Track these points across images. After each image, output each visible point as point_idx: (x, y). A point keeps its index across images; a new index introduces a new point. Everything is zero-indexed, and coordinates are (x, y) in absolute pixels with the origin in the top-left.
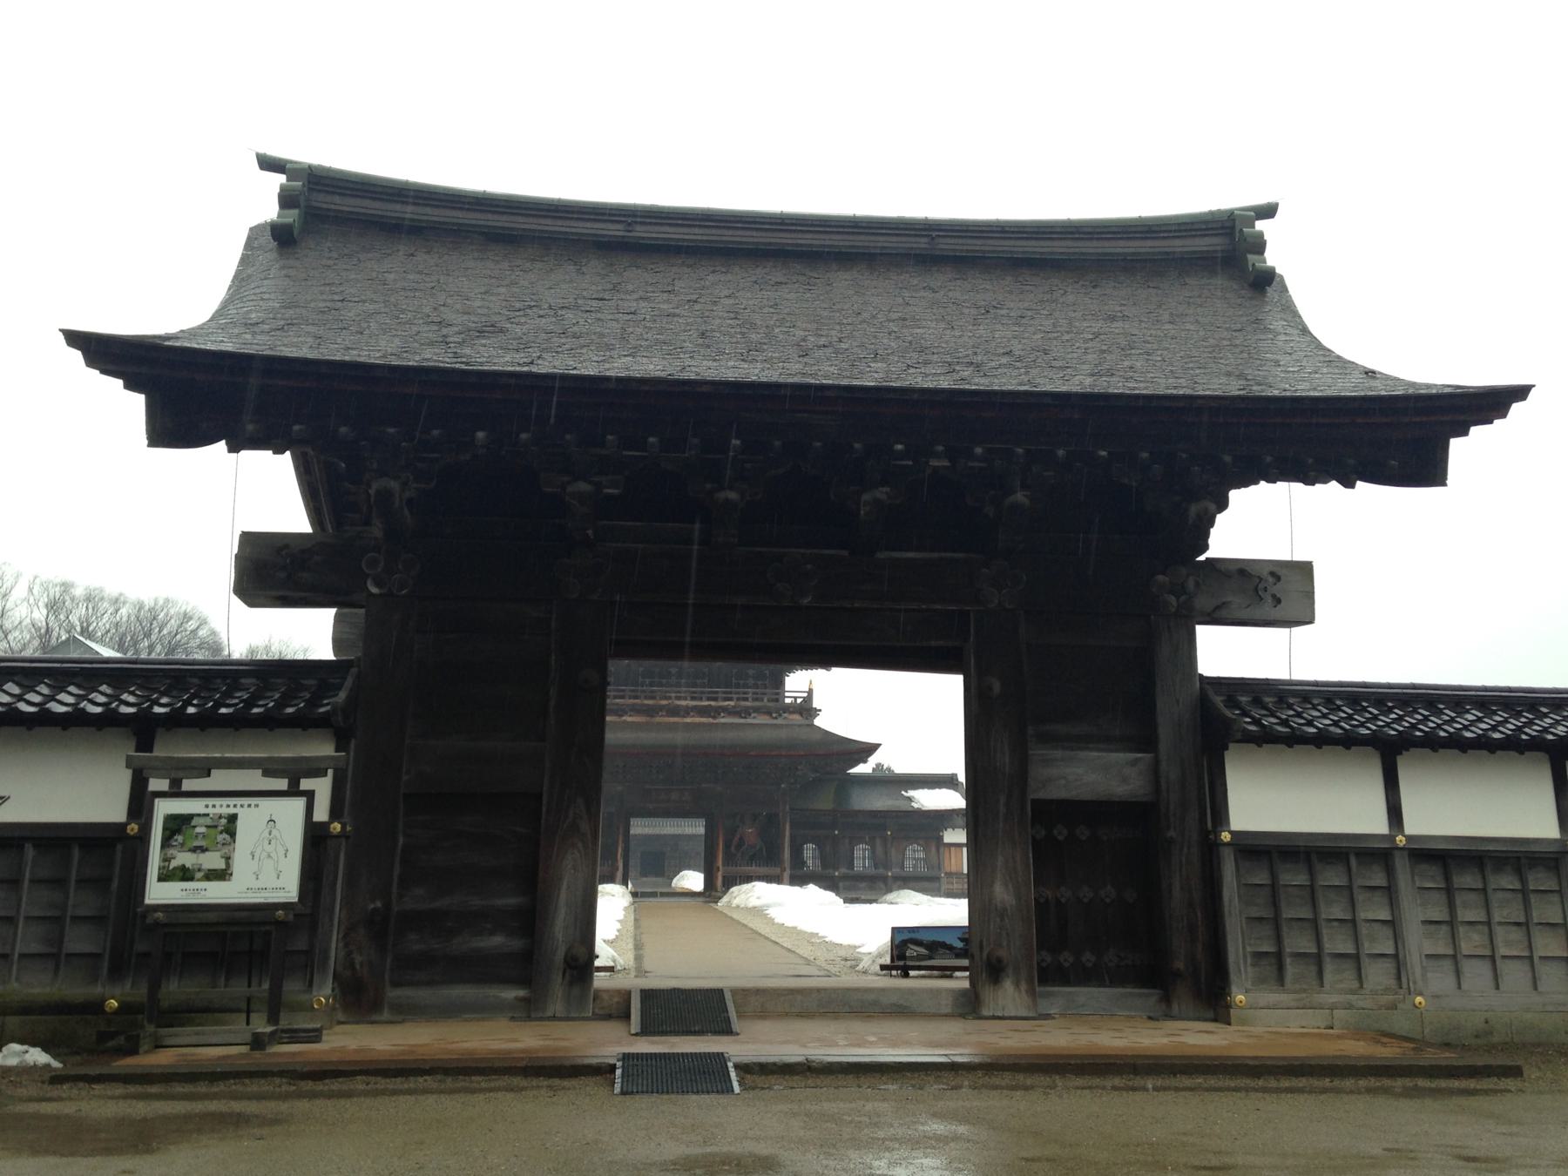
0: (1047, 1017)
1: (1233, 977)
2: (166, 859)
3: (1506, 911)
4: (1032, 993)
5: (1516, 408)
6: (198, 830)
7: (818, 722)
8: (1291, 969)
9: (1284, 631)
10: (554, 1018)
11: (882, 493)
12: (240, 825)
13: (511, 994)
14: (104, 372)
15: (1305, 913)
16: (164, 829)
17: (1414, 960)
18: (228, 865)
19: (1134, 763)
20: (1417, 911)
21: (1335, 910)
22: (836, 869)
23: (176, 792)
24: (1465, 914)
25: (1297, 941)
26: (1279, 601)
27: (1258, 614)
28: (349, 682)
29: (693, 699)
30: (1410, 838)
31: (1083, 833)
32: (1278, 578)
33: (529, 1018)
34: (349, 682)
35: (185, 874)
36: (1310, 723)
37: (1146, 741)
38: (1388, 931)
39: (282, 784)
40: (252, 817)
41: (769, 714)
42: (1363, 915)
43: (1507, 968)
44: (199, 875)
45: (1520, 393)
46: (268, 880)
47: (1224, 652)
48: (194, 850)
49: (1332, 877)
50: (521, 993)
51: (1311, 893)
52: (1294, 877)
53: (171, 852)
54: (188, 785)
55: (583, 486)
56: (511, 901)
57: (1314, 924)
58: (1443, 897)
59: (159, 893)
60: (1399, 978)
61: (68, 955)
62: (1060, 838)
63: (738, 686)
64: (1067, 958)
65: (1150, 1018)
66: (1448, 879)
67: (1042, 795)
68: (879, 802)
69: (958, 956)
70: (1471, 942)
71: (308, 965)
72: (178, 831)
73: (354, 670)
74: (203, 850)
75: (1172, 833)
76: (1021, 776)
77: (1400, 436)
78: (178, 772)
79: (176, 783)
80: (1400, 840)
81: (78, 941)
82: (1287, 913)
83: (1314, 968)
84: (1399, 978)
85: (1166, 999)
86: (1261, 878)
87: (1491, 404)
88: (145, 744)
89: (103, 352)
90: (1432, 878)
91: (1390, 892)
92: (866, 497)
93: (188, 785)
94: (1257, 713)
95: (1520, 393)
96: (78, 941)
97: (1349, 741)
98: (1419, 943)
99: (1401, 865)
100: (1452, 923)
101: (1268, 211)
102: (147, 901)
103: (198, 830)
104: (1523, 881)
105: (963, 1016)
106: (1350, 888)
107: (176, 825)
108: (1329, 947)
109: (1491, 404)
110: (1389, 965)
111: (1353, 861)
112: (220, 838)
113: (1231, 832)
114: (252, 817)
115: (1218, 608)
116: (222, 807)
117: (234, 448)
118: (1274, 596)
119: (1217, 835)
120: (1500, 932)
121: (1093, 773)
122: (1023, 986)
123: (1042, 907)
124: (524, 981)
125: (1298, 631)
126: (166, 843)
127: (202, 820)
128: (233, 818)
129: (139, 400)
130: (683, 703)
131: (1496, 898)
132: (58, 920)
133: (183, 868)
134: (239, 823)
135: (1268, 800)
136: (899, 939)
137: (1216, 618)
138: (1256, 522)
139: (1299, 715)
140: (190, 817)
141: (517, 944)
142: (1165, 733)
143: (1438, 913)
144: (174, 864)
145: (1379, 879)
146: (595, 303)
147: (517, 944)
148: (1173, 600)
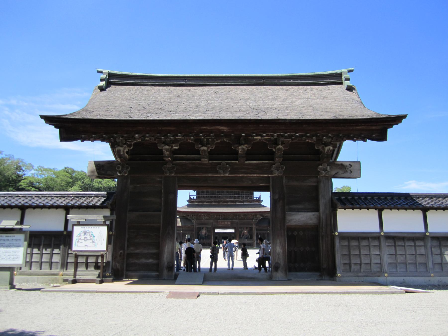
0: (291, 280)
1: (338, 269)
4: (286, 274)
8: (353, 266)
9: (355, 180)
10: (165, 280)
11: (245, 147)
14: (49, 124)
15: (357, 253)
19: (314, 215)
21: (364, 252)
24: (398, 252)
26: (351, 172)
29: (230, 198)
30: (385, 233)
32: (351, 166)
33: (158, 280)
37: (317, 210)
45: (404, 117)
47: (339, 184)
51: (359, 247)
52: (354, 243)
56: (154, 251)
57: (360, 255)
58: (393, 248)
62: (295, 235)
63: (241, 195)
65: (317, 280)
67: (289, 224)
73: (115, 194)
76: (284, 218)
80: (382, 234)
82: (352, 252)
85: (321, 276)
86: (346, 243)
87: (397, 120)
88: (67, 213)
89: (49, 120)
91: (379, 247)
92: (240, 147)
95: (404, 117)
97: (10, 207)
99: (382, 240)
100: (396, 255)
104: (415, 243)
109: (397, 120)
111: (370, 240)
113: (338, 232)
115: (336, 173)
117: (82, 141)
118: (350, 171)
123: (290, 253)
124: (157, 271)
125: (358, 179)
130: (228, 199)
135: (349, 221)
141: (155, 262)
143: (393, 252)
148: (323, 172)
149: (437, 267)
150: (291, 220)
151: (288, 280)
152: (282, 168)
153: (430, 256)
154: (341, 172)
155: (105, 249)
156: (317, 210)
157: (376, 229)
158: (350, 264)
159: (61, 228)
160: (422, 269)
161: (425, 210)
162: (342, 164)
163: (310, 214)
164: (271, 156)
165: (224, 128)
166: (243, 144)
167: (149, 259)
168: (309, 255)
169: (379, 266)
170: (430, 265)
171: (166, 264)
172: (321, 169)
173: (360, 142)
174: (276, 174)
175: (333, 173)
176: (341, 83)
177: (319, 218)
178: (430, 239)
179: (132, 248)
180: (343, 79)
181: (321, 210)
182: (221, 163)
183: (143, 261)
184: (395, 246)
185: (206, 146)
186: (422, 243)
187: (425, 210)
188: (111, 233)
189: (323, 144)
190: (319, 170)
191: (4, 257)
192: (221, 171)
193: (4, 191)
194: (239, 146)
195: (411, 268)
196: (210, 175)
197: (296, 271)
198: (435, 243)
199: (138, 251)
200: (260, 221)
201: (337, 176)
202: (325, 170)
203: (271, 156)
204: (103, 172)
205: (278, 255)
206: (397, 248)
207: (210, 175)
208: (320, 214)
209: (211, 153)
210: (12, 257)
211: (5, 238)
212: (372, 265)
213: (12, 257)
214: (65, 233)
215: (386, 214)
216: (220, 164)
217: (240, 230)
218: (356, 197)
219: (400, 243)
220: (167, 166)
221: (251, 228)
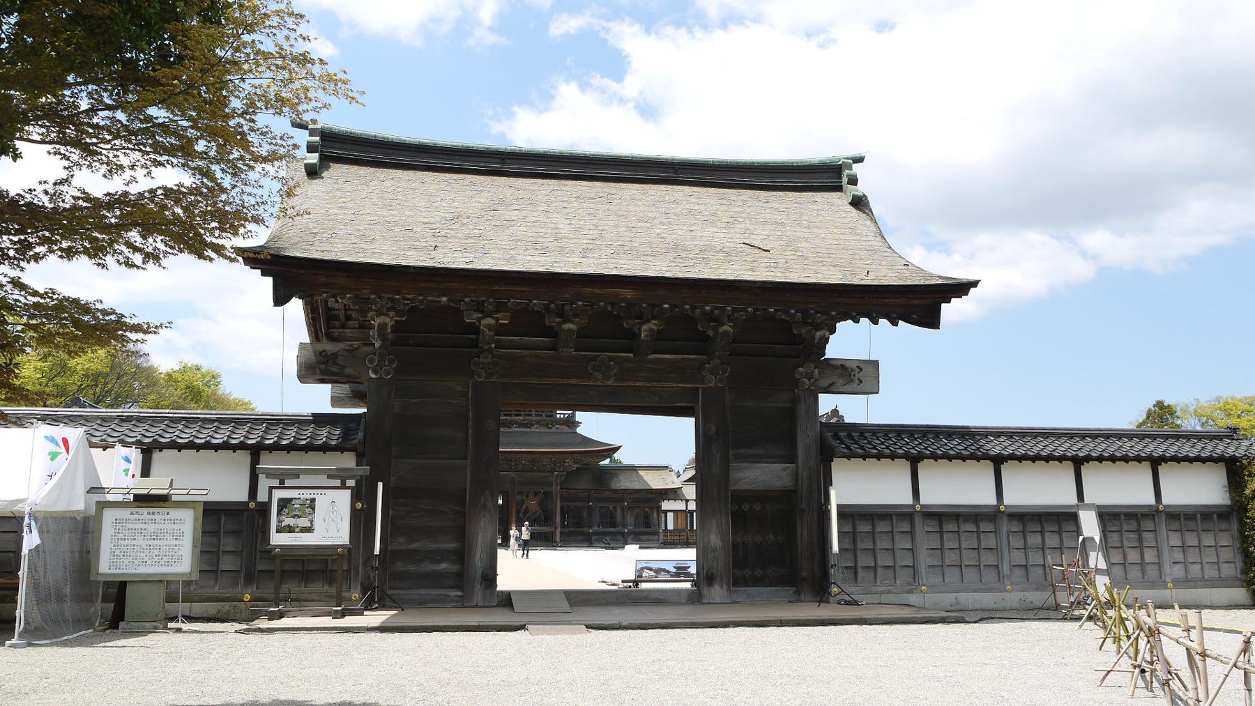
2: (280, 522)
3: (969, 541)
4: (729, 590)
5: (972, 290)
7: (579, 430)
8: (861, 573)
10: (476, 606)
11: (653, 325)
17: (923, 569)
19: (784, 470)
21: (883, 543)
22: (590, 527)
23: (282, 487)
24: (947, 545)
25: (865, 560)
27: (848, 388)
28: (362, 427)
30: (922, 506)
31: (757, 507)
34: (362, 427)
35: (290, 529)
36: (875, 448)
37: (792, 459)
38: (910, 554)
39: (338, 483)
40: (324, 500)
41: (547, 425)
42: (898, 546)
45: (975, 284)
48: (294, 517)
49: (883, 527)
50: (459, 593)
54: (288, 483)
55: (490, 321)
56: (452, 545)
58: (938, 535)
64: (748, 572)
66: (941, 527)
67: (736, 487)
68: (625, 483)
70: (951, 557)
71: (348, 575)
75: (803, 506)
77: (920, 303)
78: (282, 478)
79: (282, 482)
80: (1002, 508)
81: (227, 563)
82: (860, 545)
85: (798, 593)
90: (932, 526)
91: (912, 533)
92: (645, 327)
94: (848, 441)
95: (975, 284)
96: (227, 563)
98: (925, 559)
99: (918, 520)
101: (859, 160)
104: (978, 527)
105: (693, 603)
107: (284, 504)
108: (880, 563)
109: (961, 288)
114: (324, 500)
115: (831, 385)
116: (307, 494)
121: (762, 474)
123: (735, 546)
124: (460, 587)
126: (279, 514)
128: (313, 500)
129: (269, 281)
131: (963, 536)
132: (216, 553)
135: (855, 486)
137: (826, 391)
138: (849, 340)
139: (869, 443)
140: (291, 499)
141: (455, 568)
143: (937, 544)
145: (906, 527)
146: (492, 213)
147: (455, 568)
149: (1019, 573)
152: (725, 371)
153: (1006, 551)
154: (840, 381)
156: (792, 459)
157: (907, 499)
158: (855, 569)
159: (241, 495)
160: (990, 576)
161: (998, 461)
163: (778, 467)
164: (702, 344)
165: (628, 293)
166: (648, 321)
168: (772, 550)
169: (910, 571)
170: (1006, 568)
171: (479, 574)
172: (801, 374)
174: (712, 381)
175: (824, 383)
176: (839, 188)
177: (796, 476)
179: (401, 540)
180: (845, 180)
183: (429, 567)
184: (941, 533)
185: (572, 322)
186: (990, 527)
187: (998, 461)
188: (359, 505)
189: (811, 325)
190: (797, 376)
191: (146, 559)
192: (598, 375)
193: (19, 405)
194: (641, 324)
195: (970, 575)
196: (573, 382)
197: (747, 586)
198: (1016, 527)
199: (413, 546)
200: (573, 475)
201: (832, 388)
202: (810, 376)
203: (702, 344)
204: (334, 369)
205: (714, 550)
206: (945, 536)
207: (573, 382)
209: (581, 333)
210: (166, 559)
211: (145, 516)
212: (898, 569)
213: (166, 559)
215: (927, 472)
216: (595, 358)
217: (518, 498)
218: (854, 434)
219: (950, 527)
221: (548, 495)
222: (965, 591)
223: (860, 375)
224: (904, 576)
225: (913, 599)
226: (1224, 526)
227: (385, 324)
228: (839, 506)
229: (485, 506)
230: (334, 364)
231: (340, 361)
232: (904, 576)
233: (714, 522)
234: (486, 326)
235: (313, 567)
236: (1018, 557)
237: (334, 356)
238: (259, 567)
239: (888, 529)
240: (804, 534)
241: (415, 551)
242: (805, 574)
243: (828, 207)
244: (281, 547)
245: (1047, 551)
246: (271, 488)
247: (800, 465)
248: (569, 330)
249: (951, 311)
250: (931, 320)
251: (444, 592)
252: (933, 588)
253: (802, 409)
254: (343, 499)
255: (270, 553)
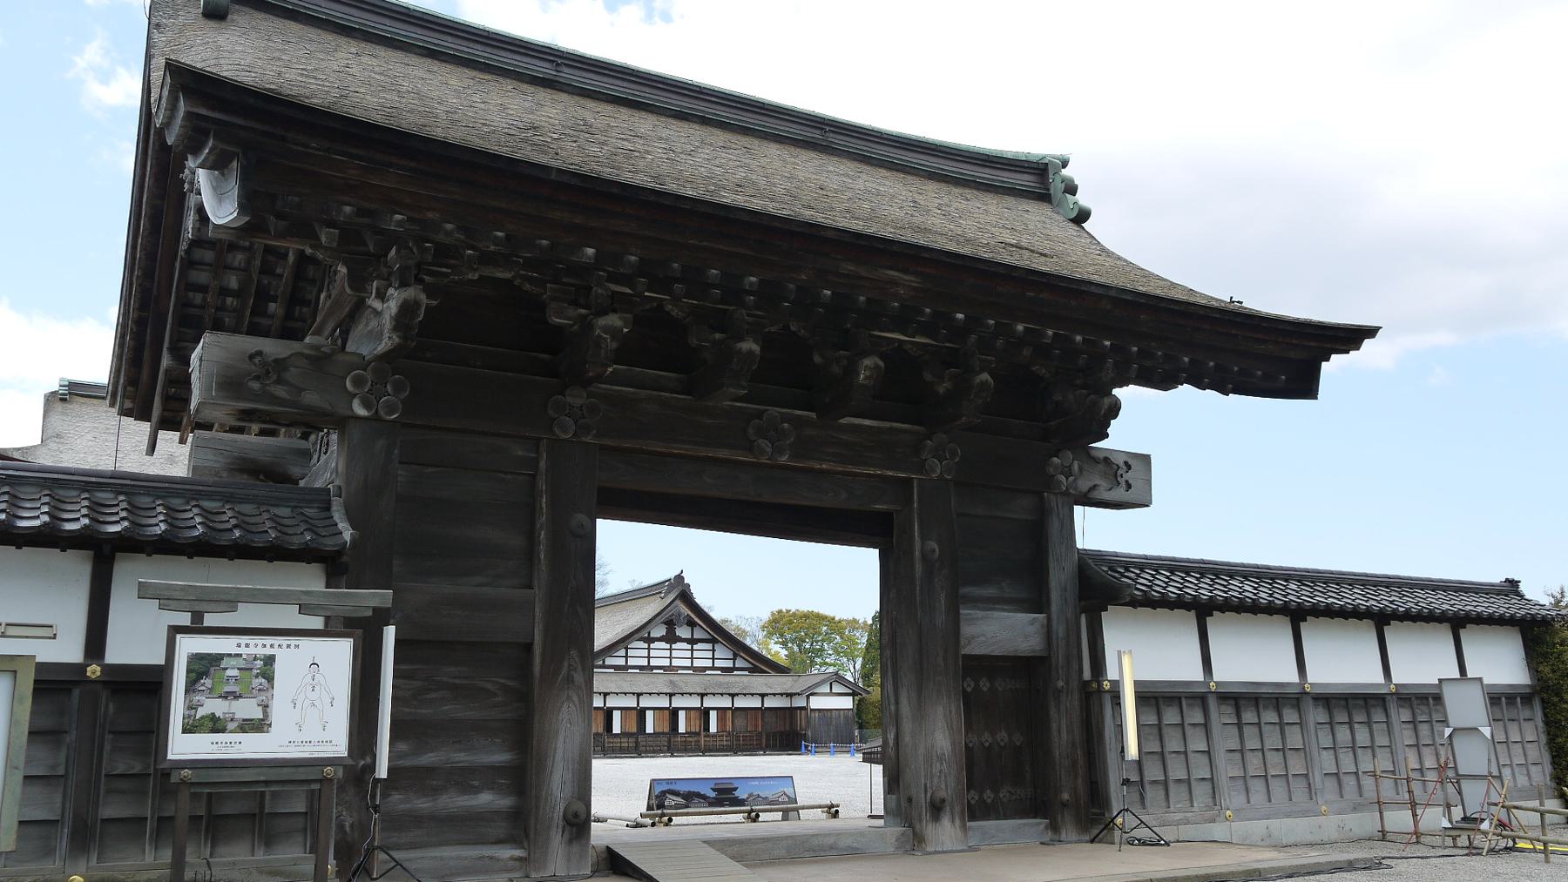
2: (192, 707)
4: (964, 828)
6: (229, 673)
12: (279, 668)
13: (508, 853)
16: (189, 671)
17: (1223, 782)
18: (266, 713)
19: (1032, 622)
20: (1225, 739)
23: (197, 628)
32: (1129, 467)
35: (215, 725)
37: (1037, 602)
43: (1273, 783)
44: (231, 726)
45: (1371, 332)
46: (313, 732)
48: (225, 696)
50: (518, 853)
53: (197, 698)
56: (500, 757)
58: (1235, 730)
59: (183, 746)
60: (1214, 797)
61: (103, 821)
66: (1239, 716)
69: (711, 805)
70: (1254, 762)
72: (206, 674)
74: (237, 697)
75: (1060, 684)
77: (1278, 356)
79: (198, 616)
83: (1162, 793)
84: (1214, 797)
85: (1054, 828)
87: (1350, 337)
91: (1206, 726)
93: (210, 620)
95: (1371, 332)
98: (1228, 768)
99: (1212, 703)
102: (170, 757)
103: (229, 673)
106: (1182, 725)
107: (203, 667)
109: (1350, 337)
110: (1207, 786)
111: (1184, 702)
112: (257, 682)
114: (293, 658)
116: (257, 646)
119: (1100, 684)
120: (1269, 755)
121: (1001, 630)
122: (958, 822)
123: (969, 750)
126: (191, 687)
127: (233, 662)
128: (270, 660)
133: (213, 718)
134: (278, 666)
136: (658, 790)
138: (1144, 418)
141: (505, 802)
142: (1055, 596)
144: (201, 712)
147: (505, 802)
148: (1063, 478)
149: (1331, 784)
150: (973, 637)
151: (971, 849)
155: (601, 768)
157: (1196, 674)
162: (1106, 459)
167: (476, 791)
170: (1317, 778)
173: (1211, 394)
174: (937, 469)
178: (1311, 702)
181: (1054, 608)
182: (764, 411)
184: (1240, 725)
192: (764, 444)
204: (280, 391)
205: (940, 759)
208: (1049, 619)
214: (94, 671)
216: (760, 415)
219: (1249, 716)
220: (569, 399)
222: (1276, 815)
223: (1129, 476)
224: (1201, 792)
225: (1218, 830)
226: (1527, 713)
227: (417, 303)
228: (1137, 683)
229: (569, 680)
230: (279, 381)
231: (292, 374)
232: (1201, 792)
233: (940, 710)
234: (606, 329)
235: (229, 808)
236: (1327, 762)
237: (280, 364)
238: (108, 811)
239: (1177, 720)
240: (1063, 730)
241: (430, 770)
242: (1066, 796)
243: (1035, 214)
244: (195, 765)
245: (1359, 752)
246: (175, 630)
247: (1054, 617)
248: (750, 352)
249: (1333, 369)
250: (1303, 385)
251: (487, 851)
252: (1240, 815)
253: (1054, 525)
254: (339, 654)
255: (164, 779)
